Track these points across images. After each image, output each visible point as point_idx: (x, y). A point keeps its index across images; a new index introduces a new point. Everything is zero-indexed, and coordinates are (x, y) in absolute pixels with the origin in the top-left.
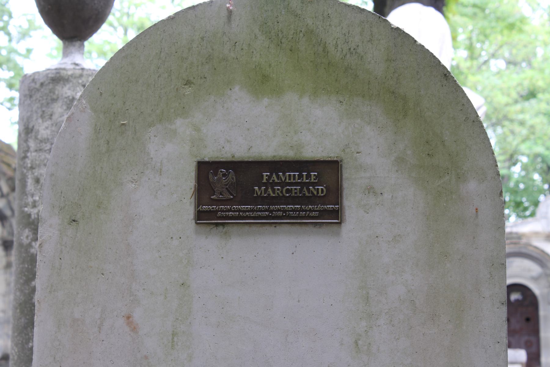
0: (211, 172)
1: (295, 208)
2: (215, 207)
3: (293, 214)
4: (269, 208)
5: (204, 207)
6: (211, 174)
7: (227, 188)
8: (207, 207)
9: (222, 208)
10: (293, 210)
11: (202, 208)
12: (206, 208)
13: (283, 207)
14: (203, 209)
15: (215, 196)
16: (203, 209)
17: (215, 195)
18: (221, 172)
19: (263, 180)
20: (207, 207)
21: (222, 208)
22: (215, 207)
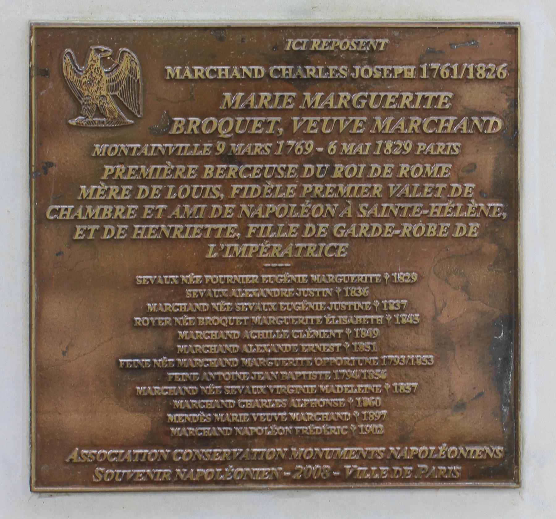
0: (69, 53)
1: (369, 452)
2: (122, 451)
3: (369, 471)
4: (289, 453)
5: (86, 452)
6: (68, 57)
7: (114, 96)
8: (95, 452)
9: (145, 455)
10: (363, 460)
11: (79, 455)
12: (93, 454)
13: (330, 451)
14: (82, 458)
15: (80, 117)
16: (83, 456)
17: (82, 115)
18: (98, 51)
19: (247, 235)
20: (95, 452)
21: (145, 455)
22: (122, 451)
